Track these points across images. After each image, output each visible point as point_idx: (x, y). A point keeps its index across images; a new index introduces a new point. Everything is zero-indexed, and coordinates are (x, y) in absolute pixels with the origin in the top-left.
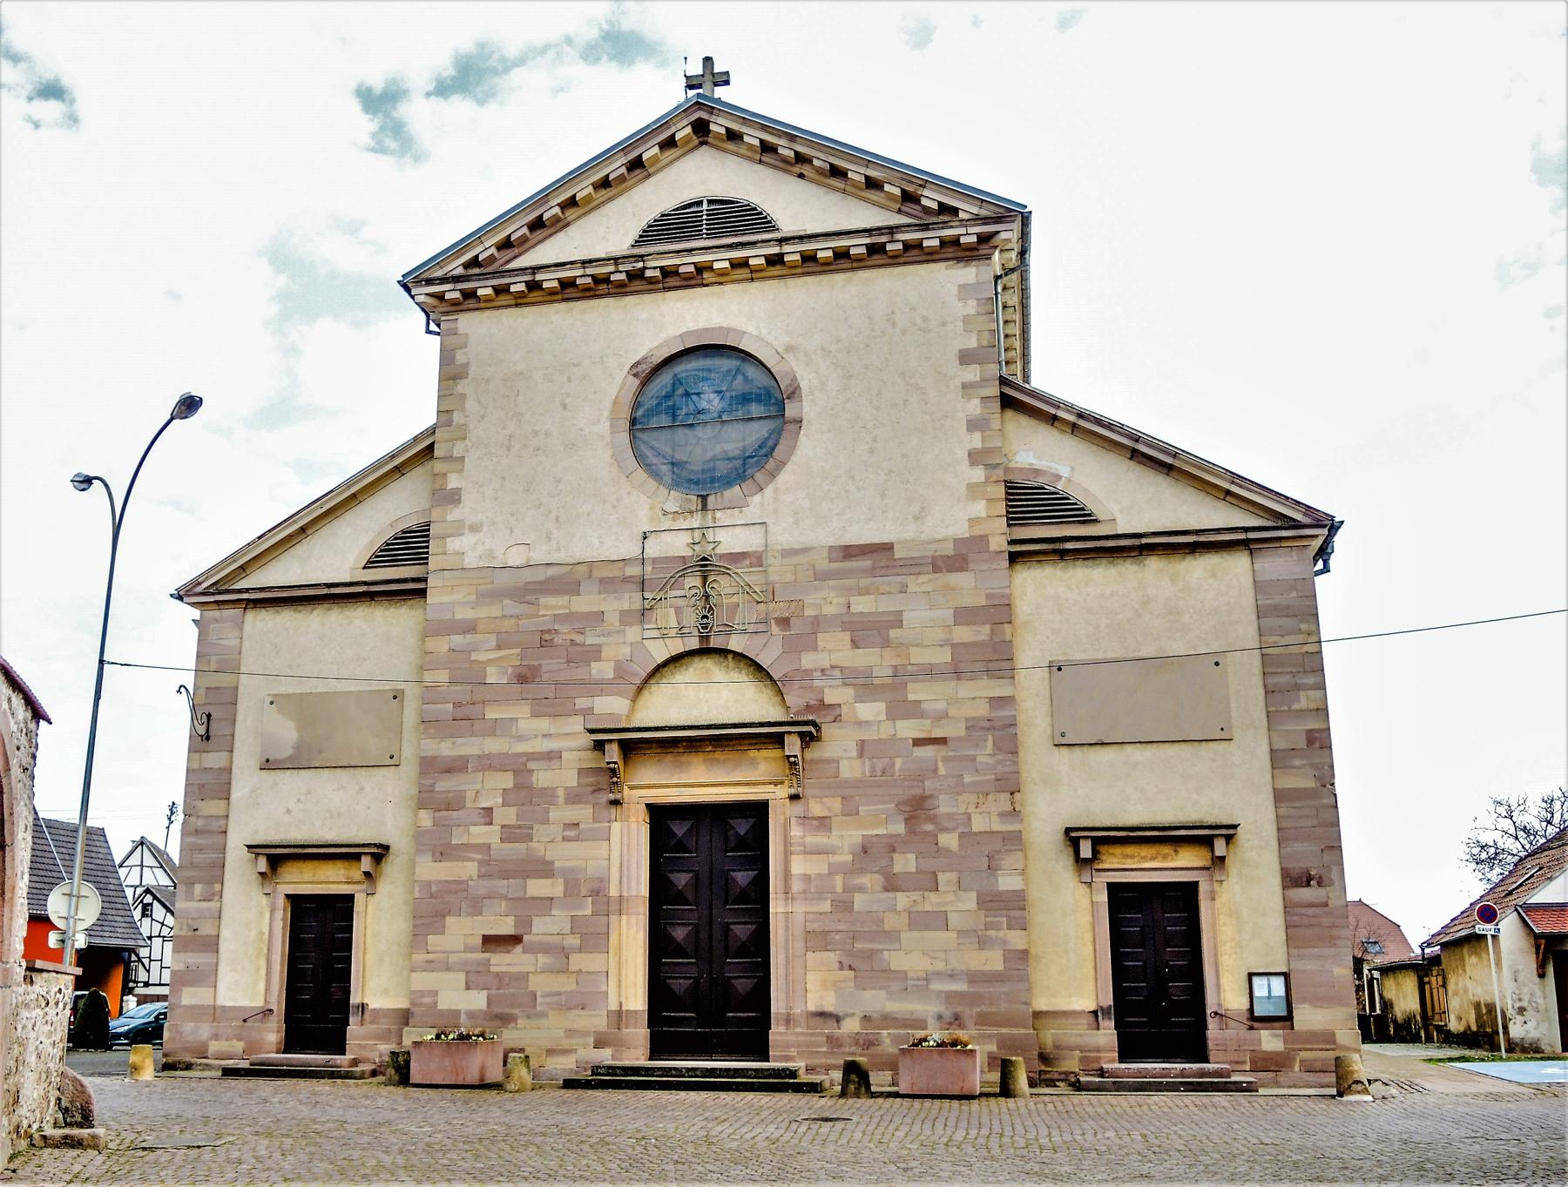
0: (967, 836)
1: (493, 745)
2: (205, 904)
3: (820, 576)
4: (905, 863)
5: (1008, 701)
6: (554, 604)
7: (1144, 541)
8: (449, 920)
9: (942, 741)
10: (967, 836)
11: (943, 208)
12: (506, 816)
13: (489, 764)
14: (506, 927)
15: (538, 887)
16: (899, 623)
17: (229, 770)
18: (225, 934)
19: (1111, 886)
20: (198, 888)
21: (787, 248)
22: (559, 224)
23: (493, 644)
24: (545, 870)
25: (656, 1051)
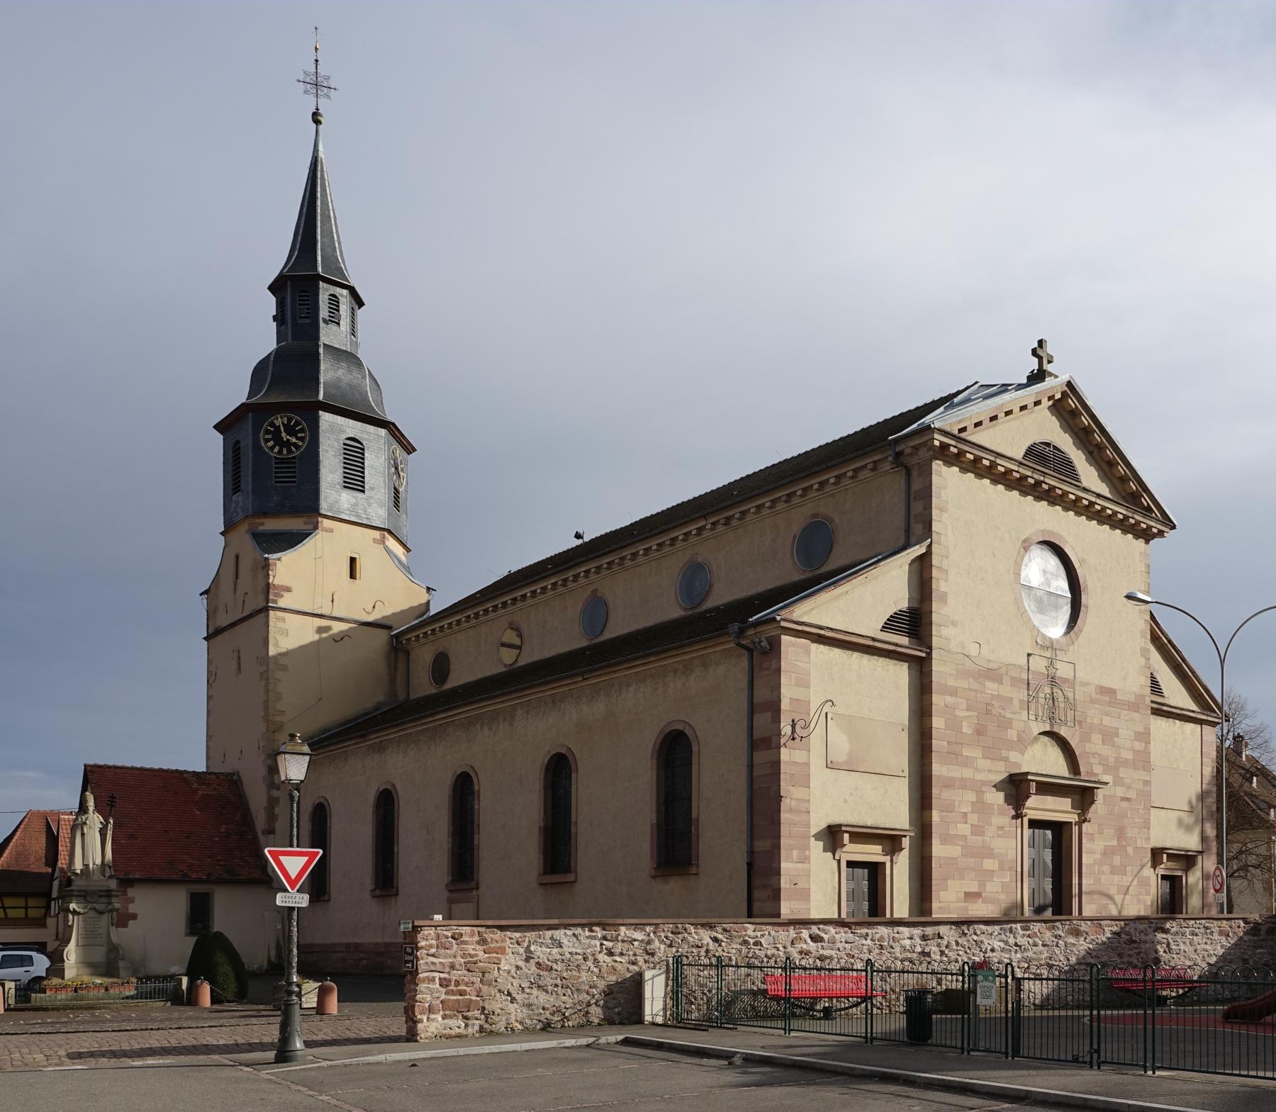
0: (1136, 848)
1: (967, 773)
2: (800, 865)
3: (1092, 701)
4: (1117, 860)
5: (1147, 783)
6: (991, 687)
7: (822, 632)
8: (950, 882)
9: (1128, 799)
10: (1136, 848)
11: (1149, 509)
12: (973, 818)
13: (964, 784)
14: (974, 889)
15: (989, 864)
16: (1117, 735)
17: (807, 765)
18: (813, 888)
19: (884, 864)
20: (795, 853)
21: (1098, 501)
22: (985, 417)
23: (964, 706)
24: (990, 853)
25: (212, 1003)
